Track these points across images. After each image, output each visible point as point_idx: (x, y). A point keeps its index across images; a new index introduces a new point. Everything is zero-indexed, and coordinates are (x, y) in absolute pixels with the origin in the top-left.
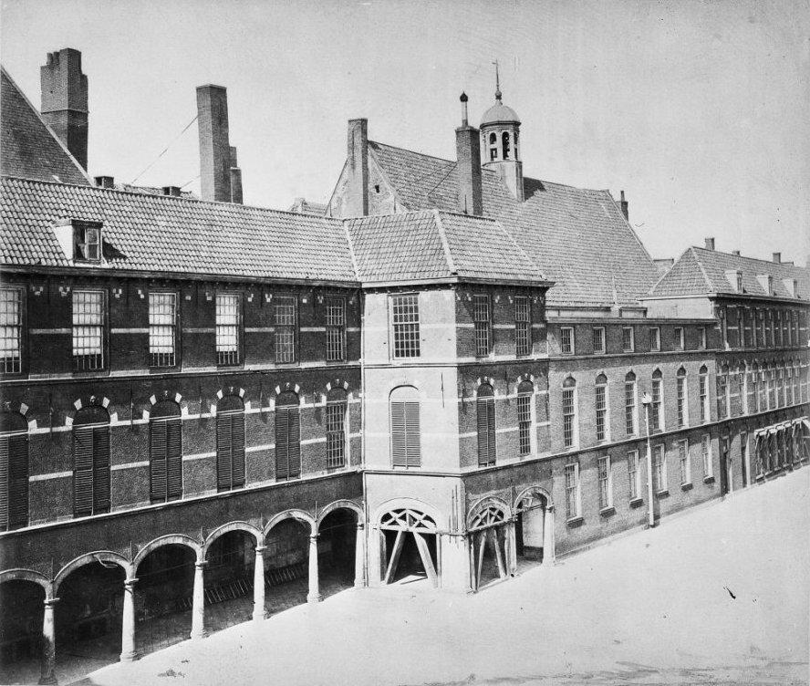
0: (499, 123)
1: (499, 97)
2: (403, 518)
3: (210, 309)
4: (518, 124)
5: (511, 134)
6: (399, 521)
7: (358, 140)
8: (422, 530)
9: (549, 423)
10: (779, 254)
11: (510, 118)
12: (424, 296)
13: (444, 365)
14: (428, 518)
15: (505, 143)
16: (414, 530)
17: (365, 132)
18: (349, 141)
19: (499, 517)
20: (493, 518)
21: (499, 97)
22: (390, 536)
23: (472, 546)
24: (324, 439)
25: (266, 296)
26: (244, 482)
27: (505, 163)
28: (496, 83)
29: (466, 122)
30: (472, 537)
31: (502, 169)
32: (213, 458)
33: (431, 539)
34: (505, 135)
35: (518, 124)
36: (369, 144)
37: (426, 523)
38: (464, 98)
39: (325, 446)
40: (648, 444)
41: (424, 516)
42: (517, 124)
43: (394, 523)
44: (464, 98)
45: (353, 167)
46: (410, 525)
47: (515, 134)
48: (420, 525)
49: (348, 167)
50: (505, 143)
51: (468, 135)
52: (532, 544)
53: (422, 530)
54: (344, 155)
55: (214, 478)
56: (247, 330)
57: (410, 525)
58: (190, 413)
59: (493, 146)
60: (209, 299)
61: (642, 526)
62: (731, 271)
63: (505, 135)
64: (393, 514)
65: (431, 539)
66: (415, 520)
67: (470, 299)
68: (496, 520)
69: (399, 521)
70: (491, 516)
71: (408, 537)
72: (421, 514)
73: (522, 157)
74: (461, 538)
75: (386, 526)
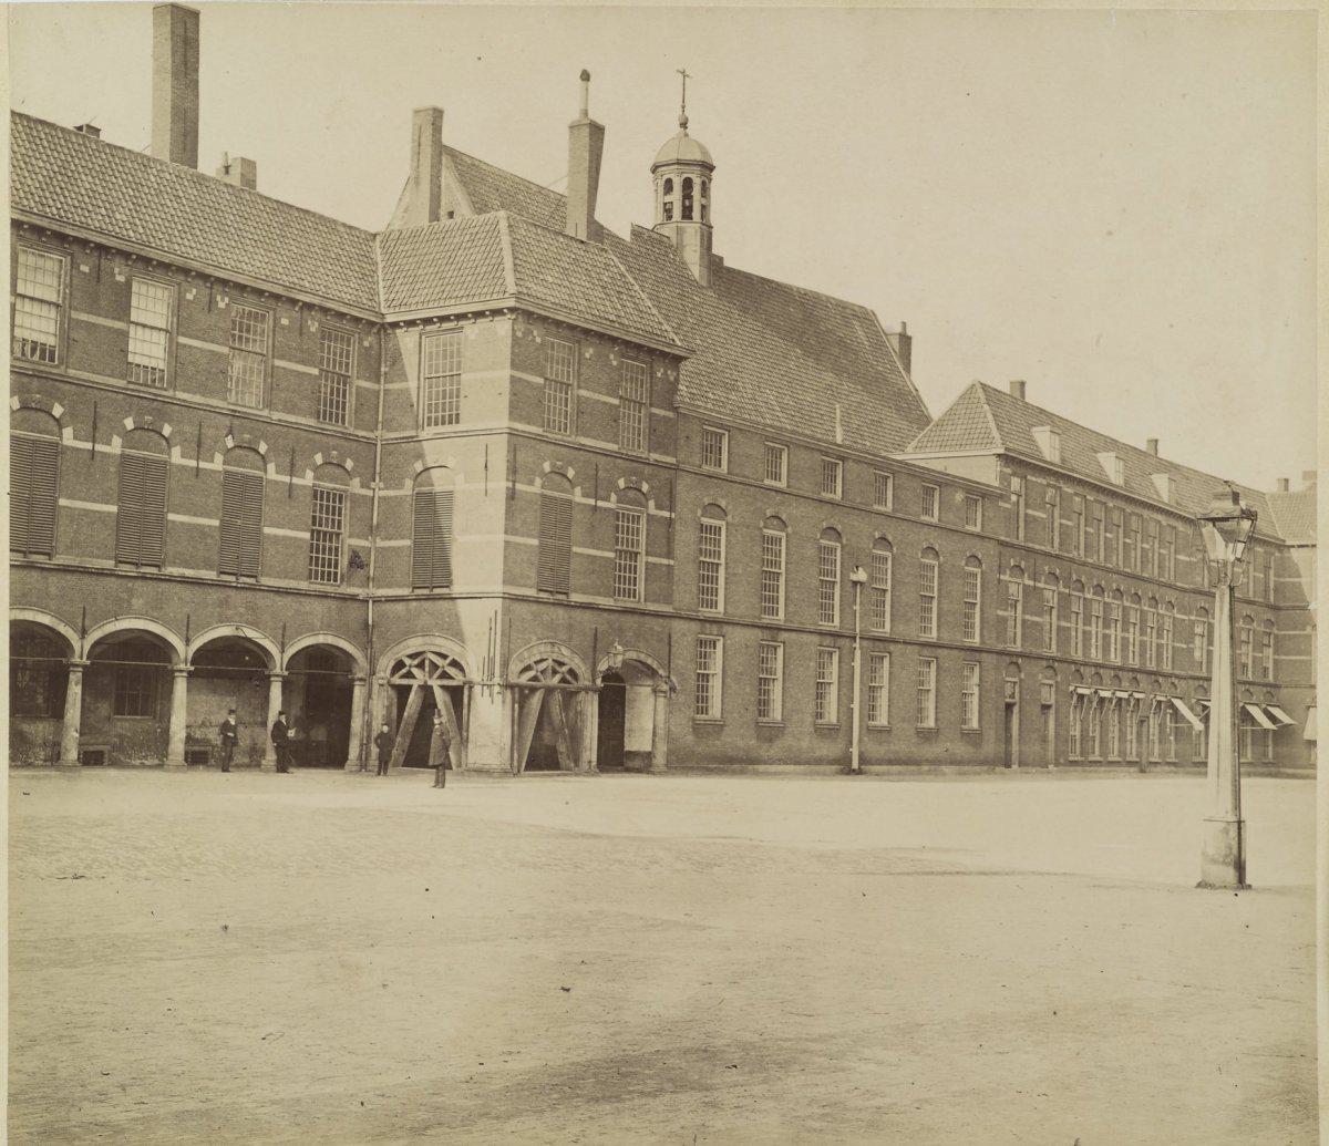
0: (679, 163)
1: (684, 125)
2: (421, 666)
3: (121, 305)
4: (711, 168)
5: (697, 181)
6: (415, 671)
7: (427, 150)
8: (446, 682)
9: (672, 562)
10: (1157, 441)
11: (698, 157)
12: (471, 330)
13: (489, 433)
14: (455, 664)
15: (687, 196)
16: (435, 683)
17: (437, 129)
18: (413, 141)
19: (569, 677)
20: (558, 677)
21: (684, 125)
22: (403, 692)
23: (516, 706)
24: (307, 535)
25: (219, 298)
26: (164, 563)
27: (686, 225)
28: (681, 103)
29: (585, 113)
30: (521, 694)
31: (680, 232)
32: (112, 513)
33: (456, 694)
34: (688, 184)
35: (711, 168)
36: (440, 149)
37: (452, 671)
38: (586, 76)
39: (306, 548)
40: (857, 645)
41: (448, 661)
42: (708, 167)
43: (409, 675)
44: (586, 76)
45: (417, 183)
46: (430, 677)
47: (703, 183)
48: (445, 675)
49: (412, 182)
50: (687, 196)
51: (586, 131)
52: (634, 749)
53: (446, 682)
54: (406, 170)
55: (111, 542)
56: (182, 340)
57: (430, 677)
58: (75, 438)
59: (668, 199)
60: (120, 278)
61: (834, 767)
62: (1042, 428)
63: (688, 184)
64: (408, 661)
65: (456, 694)
66: (437, 667)
67: (538, 340)
68: (563, 680)
69: (415, 671)
70: (555, 672)
71: (426, 690)
72: (444, 657)
73: (714, 218)
74: (497, 689)
75: (397, 680)
